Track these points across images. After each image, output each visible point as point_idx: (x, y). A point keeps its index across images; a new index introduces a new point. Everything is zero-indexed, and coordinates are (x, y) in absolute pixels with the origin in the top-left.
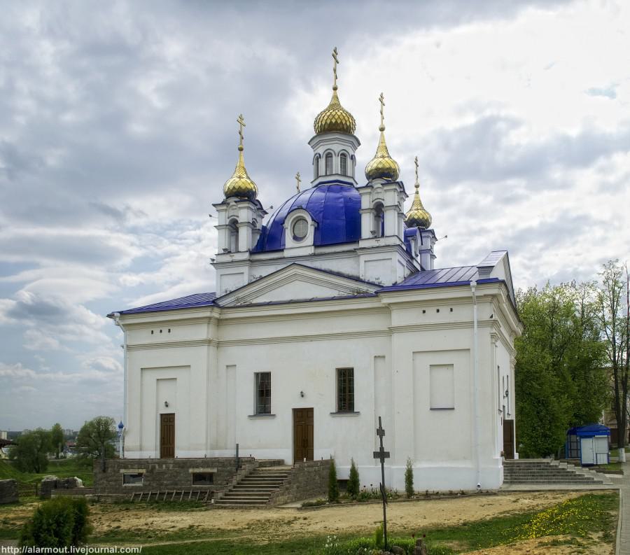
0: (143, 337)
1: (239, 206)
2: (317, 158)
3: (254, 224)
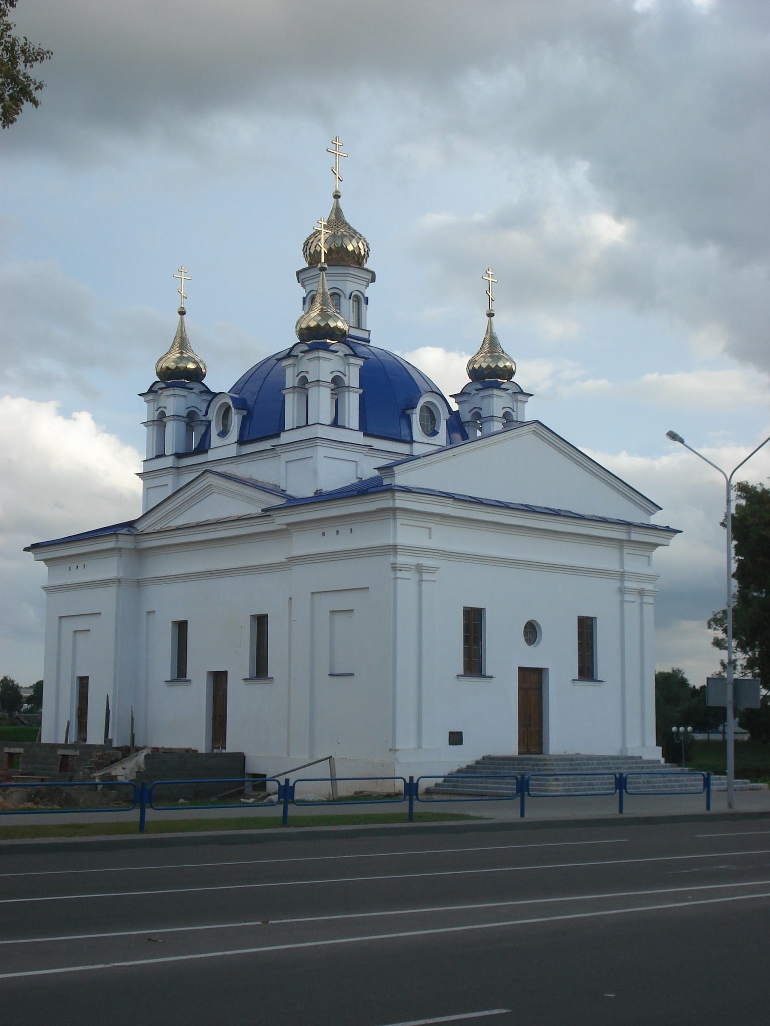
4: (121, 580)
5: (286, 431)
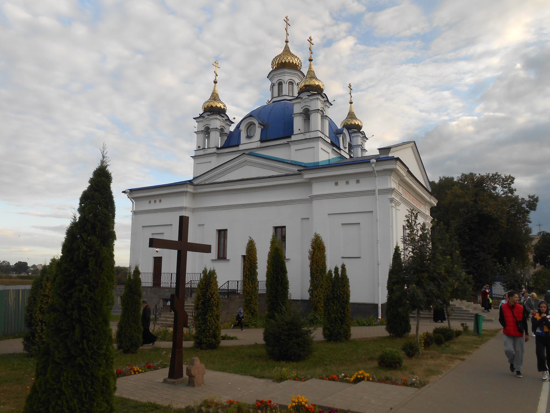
0: (145, 206)
1: (211, 118)
2: (273, 86)
3: (222, 130)
4: (187, 208)
5: (295, 135)
